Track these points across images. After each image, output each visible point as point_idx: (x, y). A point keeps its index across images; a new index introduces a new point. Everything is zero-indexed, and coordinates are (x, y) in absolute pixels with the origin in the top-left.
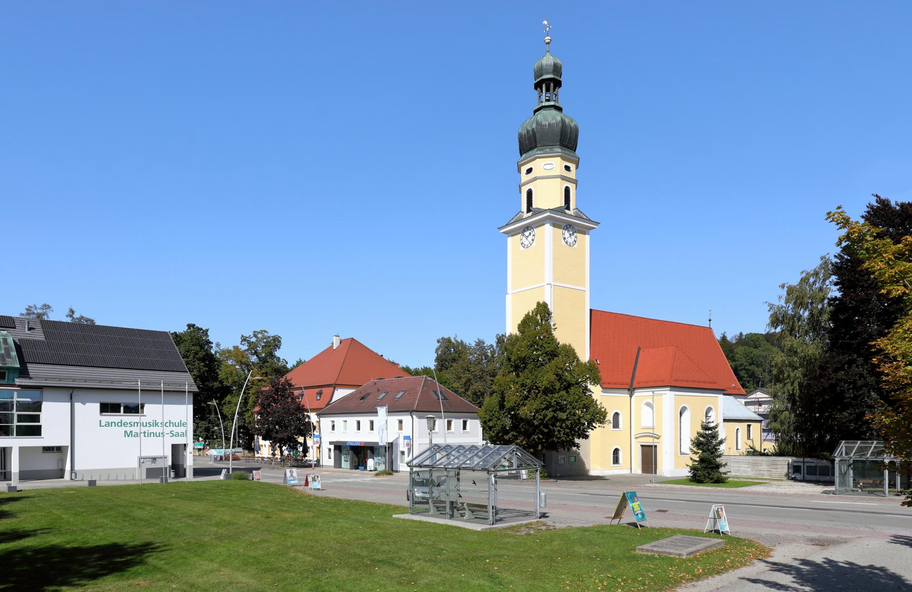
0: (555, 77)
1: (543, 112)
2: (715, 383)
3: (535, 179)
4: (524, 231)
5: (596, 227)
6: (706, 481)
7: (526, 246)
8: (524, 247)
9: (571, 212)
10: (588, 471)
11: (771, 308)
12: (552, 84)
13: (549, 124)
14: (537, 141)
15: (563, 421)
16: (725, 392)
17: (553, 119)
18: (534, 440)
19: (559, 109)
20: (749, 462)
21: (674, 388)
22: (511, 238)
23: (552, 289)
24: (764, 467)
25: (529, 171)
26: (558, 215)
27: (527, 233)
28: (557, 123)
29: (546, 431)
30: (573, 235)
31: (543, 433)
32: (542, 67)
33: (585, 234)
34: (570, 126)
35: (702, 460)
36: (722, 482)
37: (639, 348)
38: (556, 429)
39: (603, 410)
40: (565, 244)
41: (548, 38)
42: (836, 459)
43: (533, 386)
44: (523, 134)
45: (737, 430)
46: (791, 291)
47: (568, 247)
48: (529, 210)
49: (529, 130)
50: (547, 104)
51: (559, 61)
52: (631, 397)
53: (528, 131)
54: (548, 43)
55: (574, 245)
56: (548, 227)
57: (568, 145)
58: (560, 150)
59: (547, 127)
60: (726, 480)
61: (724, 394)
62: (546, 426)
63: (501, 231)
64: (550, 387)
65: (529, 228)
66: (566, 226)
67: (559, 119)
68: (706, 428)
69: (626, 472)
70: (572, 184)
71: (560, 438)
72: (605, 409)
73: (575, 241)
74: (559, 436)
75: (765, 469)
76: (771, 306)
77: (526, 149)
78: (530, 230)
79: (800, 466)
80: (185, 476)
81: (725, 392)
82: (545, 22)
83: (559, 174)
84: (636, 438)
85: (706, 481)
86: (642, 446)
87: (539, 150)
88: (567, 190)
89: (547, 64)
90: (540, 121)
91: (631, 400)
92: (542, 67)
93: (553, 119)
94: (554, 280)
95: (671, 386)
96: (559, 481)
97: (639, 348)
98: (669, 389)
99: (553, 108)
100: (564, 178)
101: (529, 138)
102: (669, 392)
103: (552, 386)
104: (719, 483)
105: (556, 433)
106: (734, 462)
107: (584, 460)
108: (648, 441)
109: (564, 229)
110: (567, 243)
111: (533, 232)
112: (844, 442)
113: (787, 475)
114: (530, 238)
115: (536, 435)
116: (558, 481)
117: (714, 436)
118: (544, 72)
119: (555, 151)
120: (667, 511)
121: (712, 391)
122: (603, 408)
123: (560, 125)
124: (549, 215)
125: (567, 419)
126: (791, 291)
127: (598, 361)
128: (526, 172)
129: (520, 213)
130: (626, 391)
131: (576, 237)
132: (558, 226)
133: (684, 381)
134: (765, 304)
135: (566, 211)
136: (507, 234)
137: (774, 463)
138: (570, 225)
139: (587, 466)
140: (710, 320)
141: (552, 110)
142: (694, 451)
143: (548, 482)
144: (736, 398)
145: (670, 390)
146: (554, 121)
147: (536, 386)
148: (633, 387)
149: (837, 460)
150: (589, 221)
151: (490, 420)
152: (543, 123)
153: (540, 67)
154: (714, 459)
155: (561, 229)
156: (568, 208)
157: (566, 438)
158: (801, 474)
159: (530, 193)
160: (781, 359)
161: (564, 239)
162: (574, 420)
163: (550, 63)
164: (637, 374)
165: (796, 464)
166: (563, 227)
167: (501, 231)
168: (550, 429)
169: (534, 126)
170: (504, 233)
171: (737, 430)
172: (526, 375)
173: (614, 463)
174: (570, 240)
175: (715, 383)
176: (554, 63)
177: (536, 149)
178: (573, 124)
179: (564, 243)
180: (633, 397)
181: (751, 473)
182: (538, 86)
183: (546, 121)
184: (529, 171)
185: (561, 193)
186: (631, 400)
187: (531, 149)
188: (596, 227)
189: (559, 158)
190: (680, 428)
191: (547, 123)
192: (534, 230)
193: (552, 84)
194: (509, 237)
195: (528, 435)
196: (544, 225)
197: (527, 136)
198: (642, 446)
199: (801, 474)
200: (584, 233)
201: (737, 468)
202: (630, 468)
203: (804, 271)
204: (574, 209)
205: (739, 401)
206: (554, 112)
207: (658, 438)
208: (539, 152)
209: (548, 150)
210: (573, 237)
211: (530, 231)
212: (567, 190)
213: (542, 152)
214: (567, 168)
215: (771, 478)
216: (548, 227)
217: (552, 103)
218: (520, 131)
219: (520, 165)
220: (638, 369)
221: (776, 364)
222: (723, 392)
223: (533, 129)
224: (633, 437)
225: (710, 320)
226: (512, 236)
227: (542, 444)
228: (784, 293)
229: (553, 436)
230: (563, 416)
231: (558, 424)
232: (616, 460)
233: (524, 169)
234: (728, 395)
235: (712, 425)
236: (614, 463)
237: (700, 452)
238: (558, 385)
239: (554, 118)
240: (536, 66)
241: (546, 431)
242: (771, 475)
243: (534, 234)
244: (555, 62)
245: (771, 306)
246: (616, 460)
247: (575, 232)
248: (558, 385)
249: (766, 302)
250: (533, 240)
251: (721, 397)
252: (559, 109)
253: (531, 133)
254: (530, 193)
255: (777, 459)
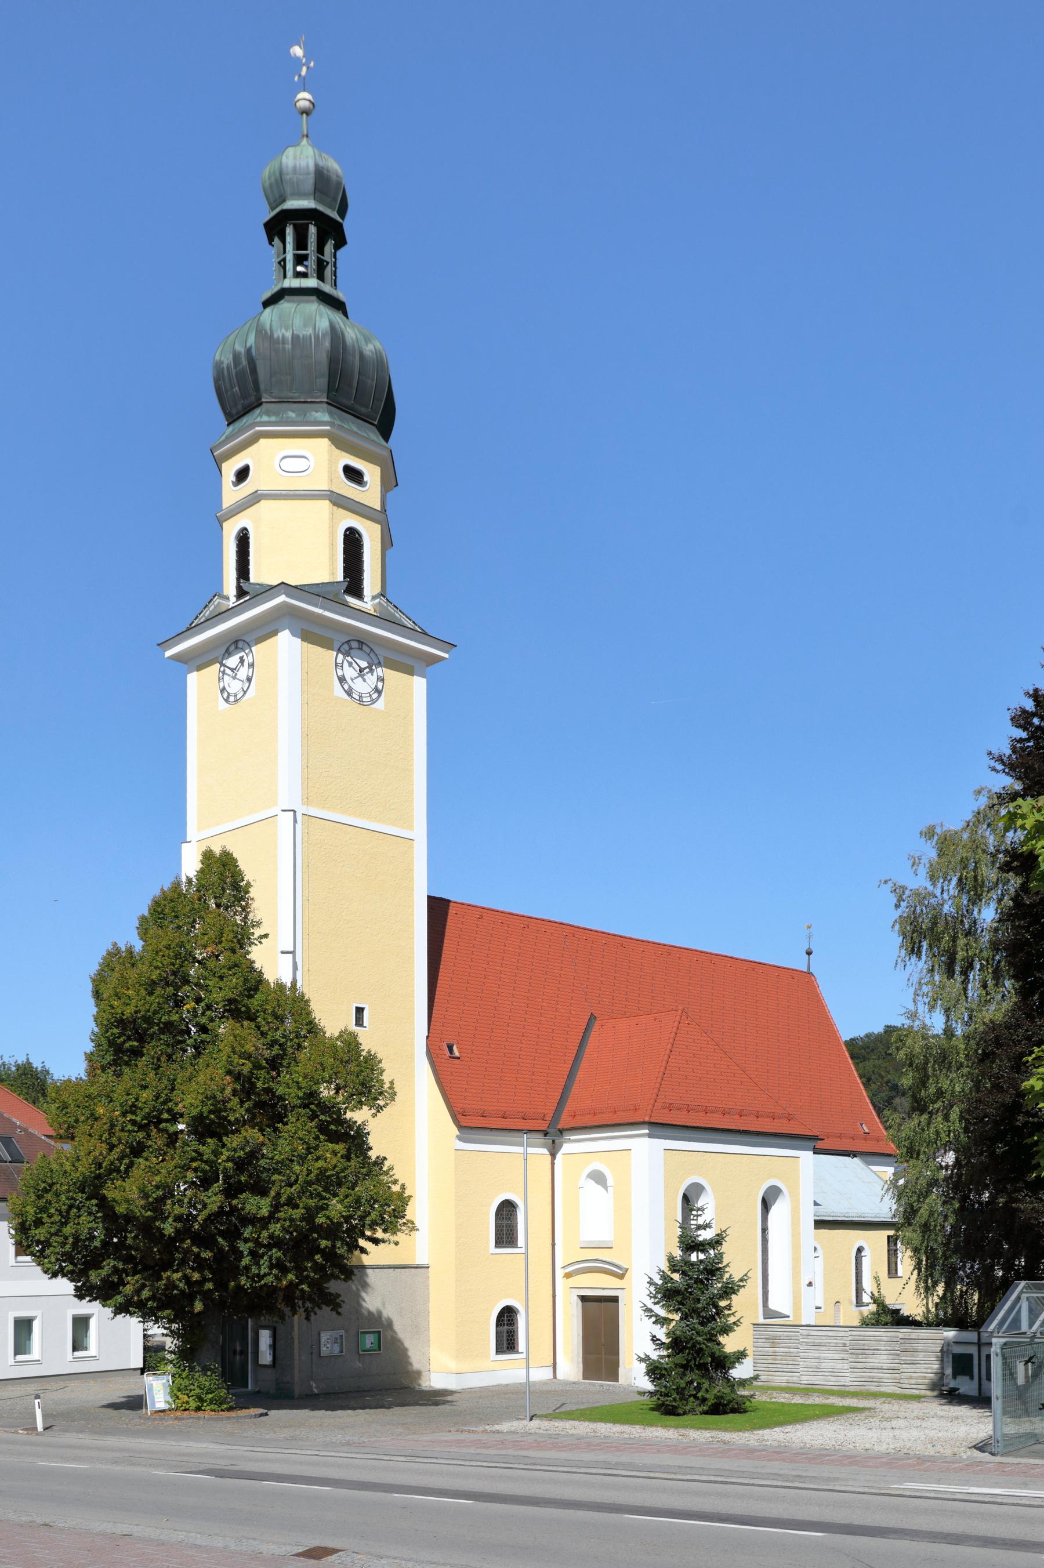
0: (321, 208)
1: (286, 305)
2: (789, 1118)
3: (255, 498)
4: (228, 653)
5: (446, 656)
6: (688, 1408)
7: (232, 699)
8: (227, 700)
9: (368, 604)
10: (419, 1373)
11: (900, 899)
12: (312, 230)
13: (295, 338)
14: (262, 387)
15: (264, 1222)
16: (819, 1145)
17: (305, 326)
18: (171, 1285)
19: (337, 305)
20: (845, 1345)
21: (660, 1127)
22: (195, 673)
23: (299, 826)
24: (883, 1360)
25: (242, 474)
26: (316, 606)
27: (232, 661)
28: (317, 337)
29: (207, 1254)
30: (371, 671)
31: (201, 1265)
32: (281, 173)
33: (412, 675)
34: (362, 355)
35: (676, 1344)
36: (734, 1411)
37: (592, 1018)
38: (244, 1247)
39: (396, 1188)
40: (346, 696)
41: (304, 98)
42: (994, 1340)
43: (161, 1112)
44: (225, 365)
45: (860, 1250)
46: (946, 843)
47: (355, 705)
48: (241, 593)
49: (240, 353)
50: (296, 283)
51: (332, 165)
52: (553, 1155)
53: (236, 357)
54: (306, 112)
55: (373, 701)
56: (286, 643)
57: (357, 407)
58: (326, 418)
59: (289, 346)
60: (748, 1404)
61: (817, 1151)
62: (204, 1240)
63: (168, 653)
64: (210, 1112)
65: (240, 644)
66: (348, 642)
67: (323, 324)
68: (690, 1245)
69: (540, 1375)
70: (369, 523)
71: (261, 1277)
72: (403, 1187)
73: (379, 692)
74: (254, 1270)
75: (885, 1366)
76: (899, 892)
77: (234, 412)
78: (243, 650)
79: (971, 1356)
80: (86, 1349)
81: (819, 1145)
82: (297, 51)
83: (324, 486)
84: (568, 1276)
85: (688, 1408)
86: (584, 1299)
87: (268, 413)
88: (352, 541)
89: (295, 168)
90: (268, 327)
91: (553, 1164)
92: (281, 173)
93: (305, 326)
94: (307, 800)
95: (651, 1124)
96: (276, 1415)
97: (592, 1018)
98: (647, 1131)
99: (314, 298)
100: (339, 501)
101: (241, 376)
102: (647, 1139)
103: (216, 1111)
104: (725, 1413)
105: (246, 1261)
106: (807, 1344)
107: (407, 1344)
108: (599, 1284)
109: (339, 651)
110: (349, 693)
111: (250, 656)
112: (1023, 1283)
113: (934, 1386)
114: (243, 672)
115: (177, 1271)
116: (273, 1413)
117: (713, 1270)
118: (288, 190)
119: (312, 419)
120: (333, 1551)
121: (739, 1138)
122: (395, 1182)
123: (327, 344)
124: (284, 603)
125: (271, 1217)
126: (946, 843)
127: (455, 1048)
128: (234, 479)
129: (217, 600)
130: (539, 1139)
131: (381, 679)
132: (325, 643)
133: (779, 1118)
134: (883, 886)
135: (351, 600)
136: (185, 662)
137: (907, 1346)
138: (361, 643)
139: (416, 1361)
140: (809, 953)
141: (312, 302)
142: (657, 1316)
143: (229, 1418)
144: (868, 1164)
145: (650, 1136)
146: (310, 331)
147: (169, 1111)
148: (560, 1126)
149: (997, 1342)
150: (424, 635)
151: (38, 1223)
152: (278, 333)
153: (278, 174)
154: (710, 1340)
155: (330, 647)
156: (358, 593)
157: (276, 1277)
158: (972, 1378)
159: (243, 540)
160: (922, 1043)
161: (342, 680)
162: (292, 1220)
163: (303, 163)
164: (575, 1090)
165: (959, 1350)
166: (337, 645)
167: (168, 653)
168: (221, 1249)
169: (251, 340)
170: (176, 658)
171: (860, 1250)
172: (138, 1075)
173: (499, 1350)
174: (363, 687)
175: (789, 1118)
176: (317, 166)
177: (257, 411)
178: (370, 347)
179: (339, 691)
180: (559, 1156)
181: (849, 1379)
182: (274, 229)
183: (287, 329)
184: (242, 474)
185: (332, 544)
186: (553, 1164)
187: (248, 410)
188: (446, 656)
189: (325, 442)
190: (553, 1245)
191: (288, 335)
192: (253, 649)
193: (312, 230)
194: (190, 672)
195: (152, 1269)
196: (275, 633)
197: (234, 371)
198: (584, 1299)
199: (972, 1378)
200: (410, 671)
201: (814, 1363)
202: (551, 1363)
203: (983, 789)
204: (374, 598)
205: (874, 1172)
206: (313, 307)
207: (621, 1277)
208: (265, 418)
209: (292, 415)
210: (371, 679)
211: (242, 654)
212: (352, 541)
213: (273, 419)
214: (353, 475)
215: (898, 1391)
216: (286, 643)
217: (312, 282)
218: (217, 357)
219: (221, 455)
220: (580, 1075)
221: (911, 1057)
222: (812, 1144)
223: (249, 351)
224: (560, 1273)
225: (809, 953)
226: (199, 668)
227: (206, 1296)
228: (930, 852)
229: (236, 1271)
230: (261, 1206)
231: (247, 1232)
232: (507, 1342)
233: (230, 468)
234: (849, 1155)
235: (705, 1235)
236: (499, 1350)
237: (677, 1317)
238: (237, 1111)
239: (309, 321)
240: (266, 173)
241: (207, 1254)
242: (898, 1382)
243: (251, 661)
244: (321, 163)
245: (899, 892)
246: (507, 1342)
247: (379, 664)
248: (237, 1111)
249: (886, 882)
250: (249, 680)
251: (806, 1158)
252: (337, 305)
253: (244, 362)
254: (243, 540)
255: (913, 1336)
